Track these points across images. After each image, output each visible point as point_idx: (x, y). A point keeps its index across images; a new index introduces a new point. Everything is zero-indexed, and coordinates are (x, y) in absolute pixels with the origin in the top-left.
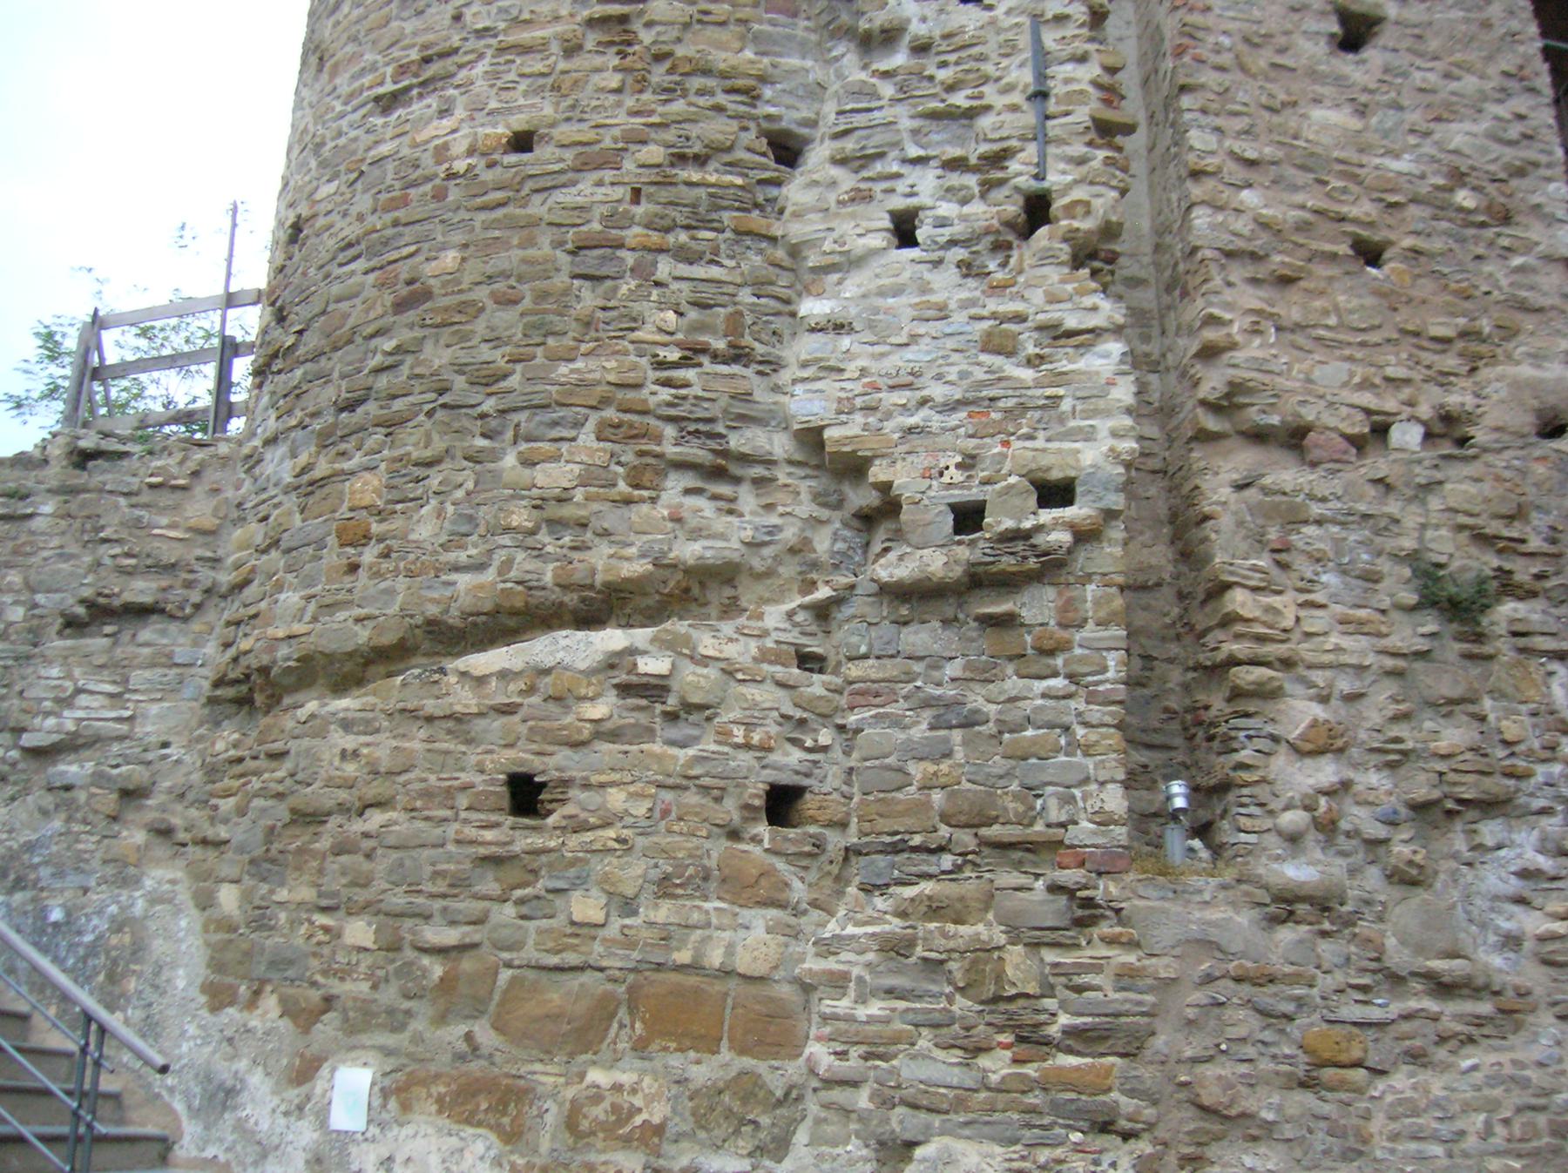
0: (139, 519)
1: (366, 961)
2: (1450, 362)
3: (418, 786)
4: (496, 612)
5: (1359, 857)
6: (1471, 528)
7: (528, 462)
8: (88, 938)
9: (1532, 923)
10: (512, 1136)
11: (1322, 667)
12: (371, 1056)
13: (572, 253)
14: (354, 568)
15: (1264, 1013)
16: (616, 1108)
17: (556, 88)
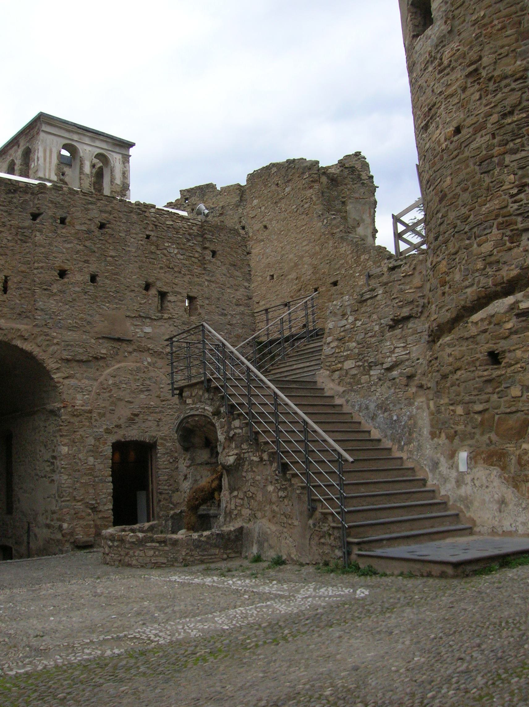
0: (401, 289)
1: (462, 418)
3: (465, 362)
4: (479, 299)
7: (479, 245)
8: (403, 423)
10: (503, 468)
12: (466, 448)
13: (480, 165)
14: (444, 294)
17: (462, 106)
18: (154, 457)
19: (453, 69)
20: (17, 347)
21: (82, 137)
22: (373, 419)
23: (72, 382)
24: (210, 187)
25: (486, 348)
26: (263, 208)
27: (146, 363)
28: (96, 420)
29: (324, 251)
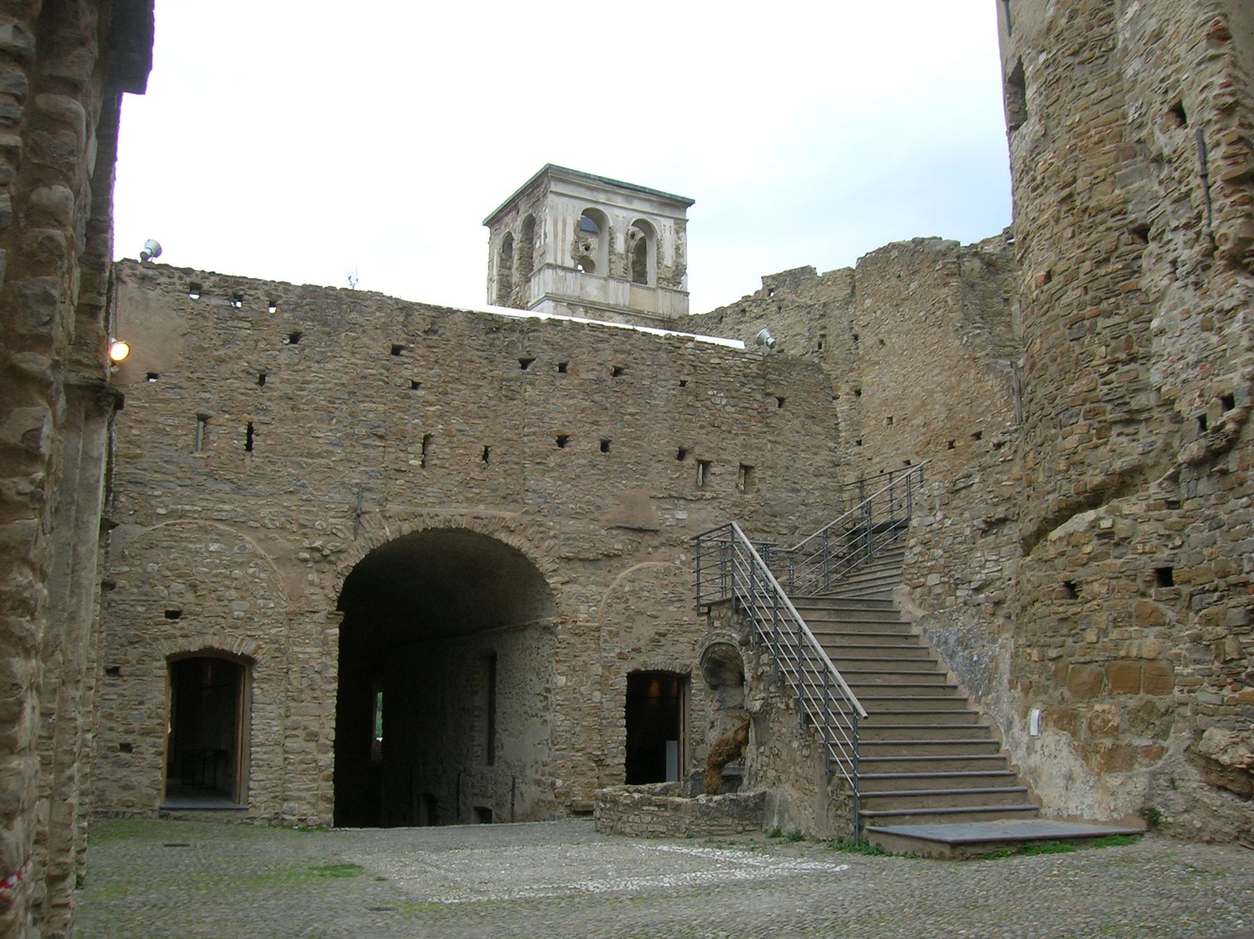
4: (1060, 510)
10: (1074, 734)
16: (1104, 720)
18: (687, 696)
19: (1047, 189)
20: (500, 541)
21: (611, 196)
22: (951, 657)
23: (574, 588)
24: (807, 271)
25: (1063, 575)
26: (879, 312)
27: (678, 562)
28: (606, 641)
29: (963, 385)
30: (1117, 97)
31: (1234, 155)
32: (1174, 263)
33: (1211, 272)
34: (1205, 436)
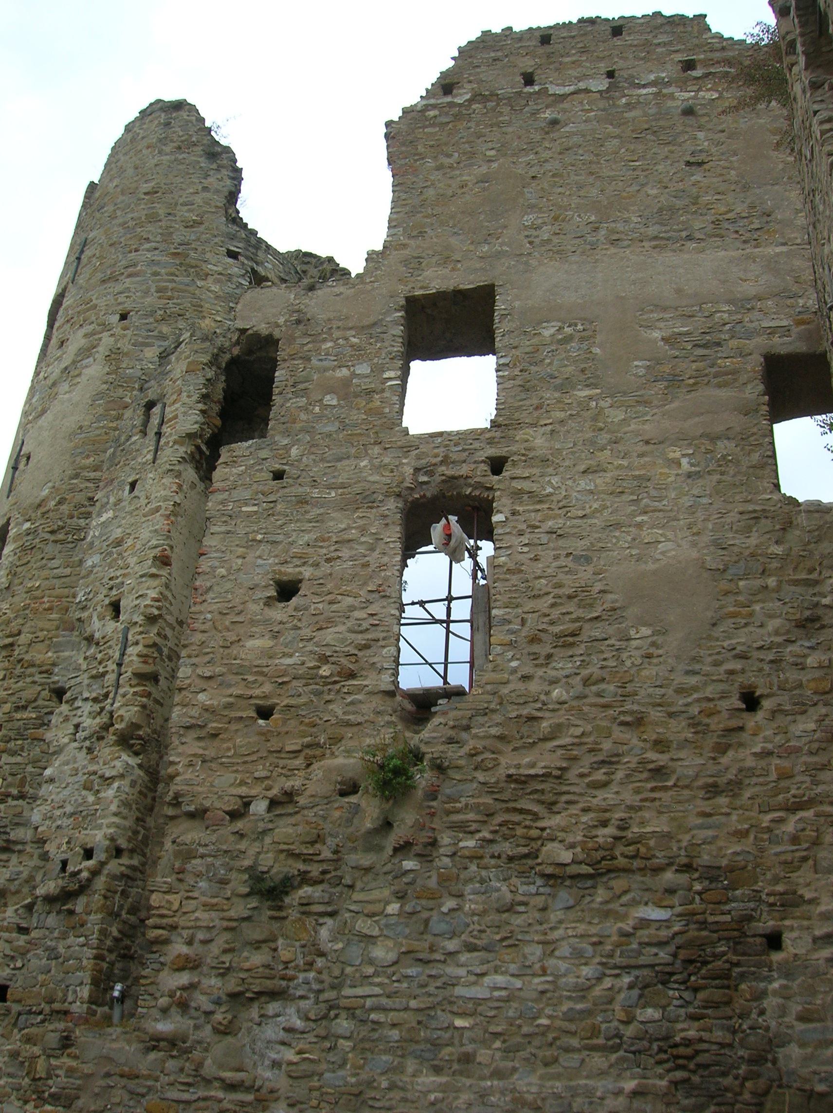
2: (299, 762)
5: (202, 1019)
6: (288, 851)
9: (290, 1055)
11: (189, 928)
15: (131, 1093)
30: (74, 578)
31: (146, 656)
32: (77, 726)
33: (103, 743)
34: (63, 878)
